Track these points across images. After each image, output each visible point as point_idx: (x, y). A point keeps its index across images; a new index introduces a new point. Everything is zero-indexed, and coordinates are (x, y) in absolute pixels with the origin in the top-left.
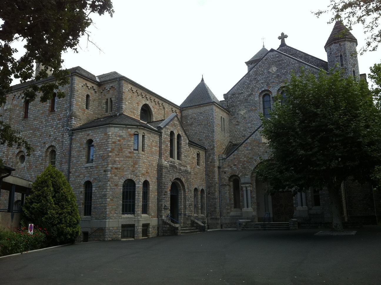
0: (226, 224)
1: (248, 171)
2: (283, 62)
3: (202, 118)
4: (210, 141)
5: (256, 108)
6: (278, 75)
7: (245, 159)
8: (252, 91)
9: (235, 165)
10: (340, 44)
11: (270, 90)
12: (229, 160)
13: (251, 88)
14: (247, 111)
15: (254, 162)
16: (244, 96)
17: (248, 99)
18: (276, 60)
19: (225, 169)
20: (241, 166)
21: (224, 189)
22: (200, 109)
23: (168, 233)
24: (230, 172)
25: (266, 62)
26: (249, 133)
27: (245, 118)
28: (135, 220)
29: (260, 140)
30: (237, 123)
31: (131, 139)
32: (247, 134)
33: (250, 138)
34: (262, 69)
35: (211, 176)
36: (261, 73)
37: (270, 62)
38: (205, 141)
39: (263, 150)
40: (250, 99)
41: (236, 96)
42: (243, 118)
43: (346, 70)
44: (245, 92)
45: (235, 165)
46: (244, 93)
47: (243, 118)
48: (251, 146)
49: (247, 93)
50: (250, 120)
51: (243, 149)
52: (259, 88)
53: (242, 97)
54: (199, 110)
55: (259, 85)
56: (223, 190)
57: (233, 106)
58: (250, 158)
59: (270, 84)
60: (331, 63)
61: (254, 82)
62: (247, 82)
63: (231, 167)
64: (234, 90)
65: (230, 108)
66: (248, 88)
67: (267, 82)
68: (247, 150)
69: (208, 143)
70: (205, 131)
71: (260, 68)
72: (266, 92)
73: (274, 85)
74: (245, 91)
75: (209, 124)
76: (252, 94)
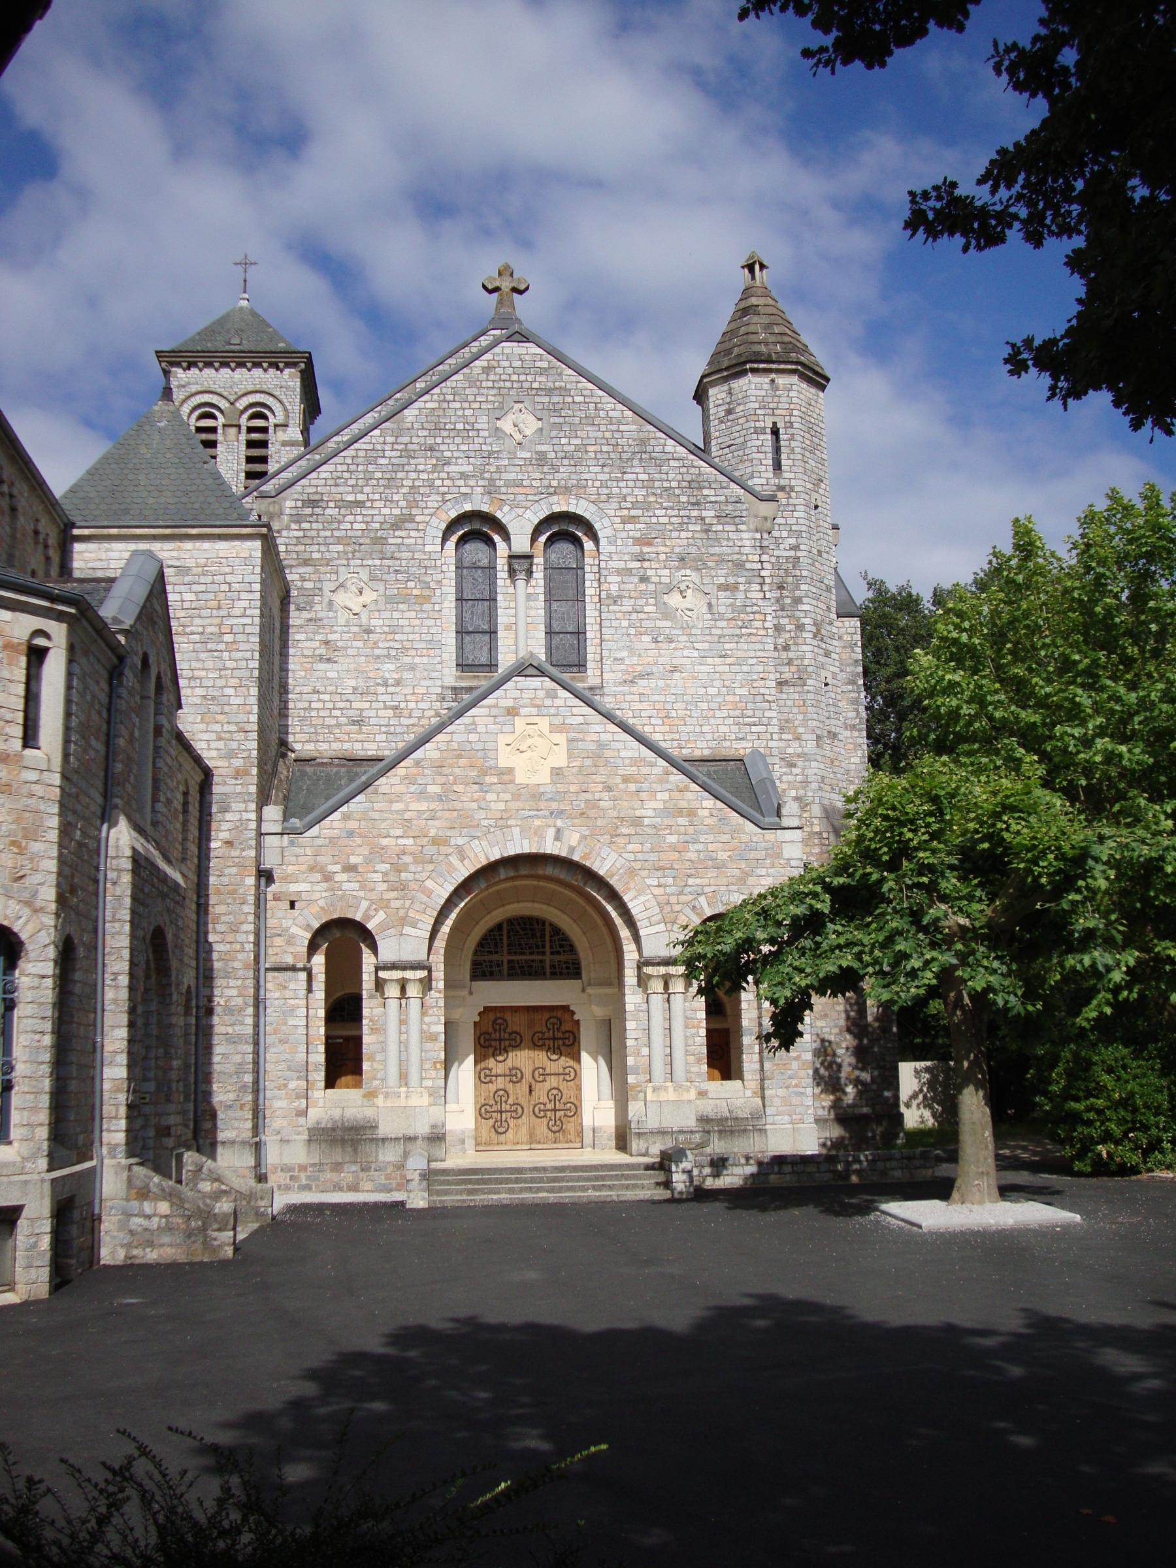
0: (286, 1169)
1: (417, 906)
2: (569, 400)
3: (189, 597)
4: (233, 728)
5: (427, 592)
6: (541, 458)
7: (401, 841)
8: (413, 504)
9: (350, 869)
10: (773, 381)
11: (499, 515)
12: (320, 841)
13: (405, 490)
14: (382, 600)
15: (454, 860)
16: (368, 519)
17: (391, 541)
18: (536, 385)
19: (293, 888)
20: (385, 874)
21: (285, 988)
22: (179, 549)
23: (162, 1245)
24: (322, 903)
25: (490, 384)
26: (386, 708)
27: (368, 631)
28: (26, 1182)
29: (490, 754)
30: (323, 651)
31: (11, 672)
32: (373, 713)
33: (439, 737)
34: (468, 412)
35: (224, 918)
36: (460, 426)
37: (508, 384)
38: (203, 727)
39: (502, 806)
40: (399, 541)
41: (328, 511)
42: (356, 629)
43: (793, 495)
44: (376, 504)
45: (350, 869)
46: (368, 504)
47: (356, 629)
48: (443, 780)
49: (386, 511)
50: (391, 644)
51: (396, 789)
52: (449, 497)
53: (356, 526)
54: (175, 554)
55: (446, 482)
56: (277, 995)
57: (306, 562)
58: (435, 841)
59: (504, 490)
60: (727, 450)
61: (424, 463)
62: (387, 454)
63: (328, 878)
64: (314, 482)
65: (292, 566)
66: (391, 483)
67: (486, 475)
68: (422, 795)
69: (220, 739)
70: (203, 673)
71: (458, 405)
72: (476, 525)
73: (520, 498)
74: (377, 496)
75: (228, 638)
76: (411, 519)
